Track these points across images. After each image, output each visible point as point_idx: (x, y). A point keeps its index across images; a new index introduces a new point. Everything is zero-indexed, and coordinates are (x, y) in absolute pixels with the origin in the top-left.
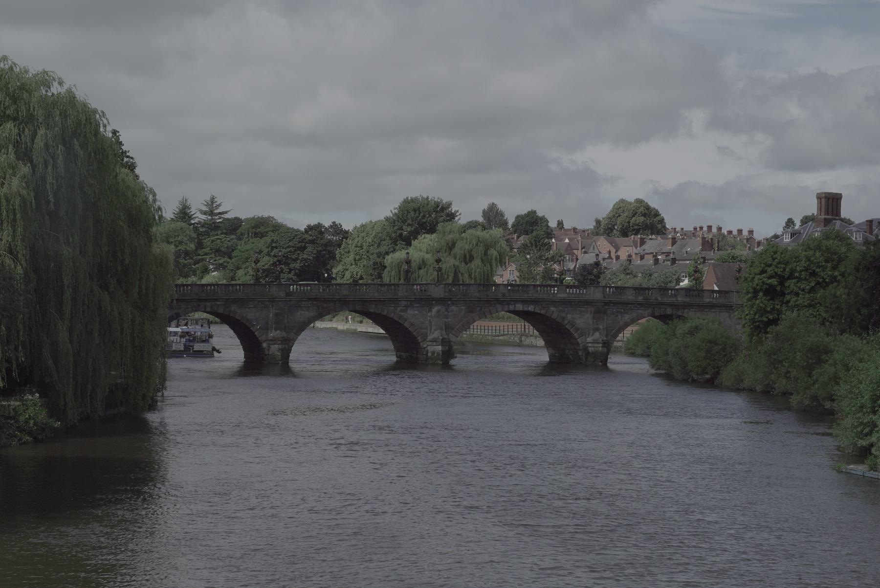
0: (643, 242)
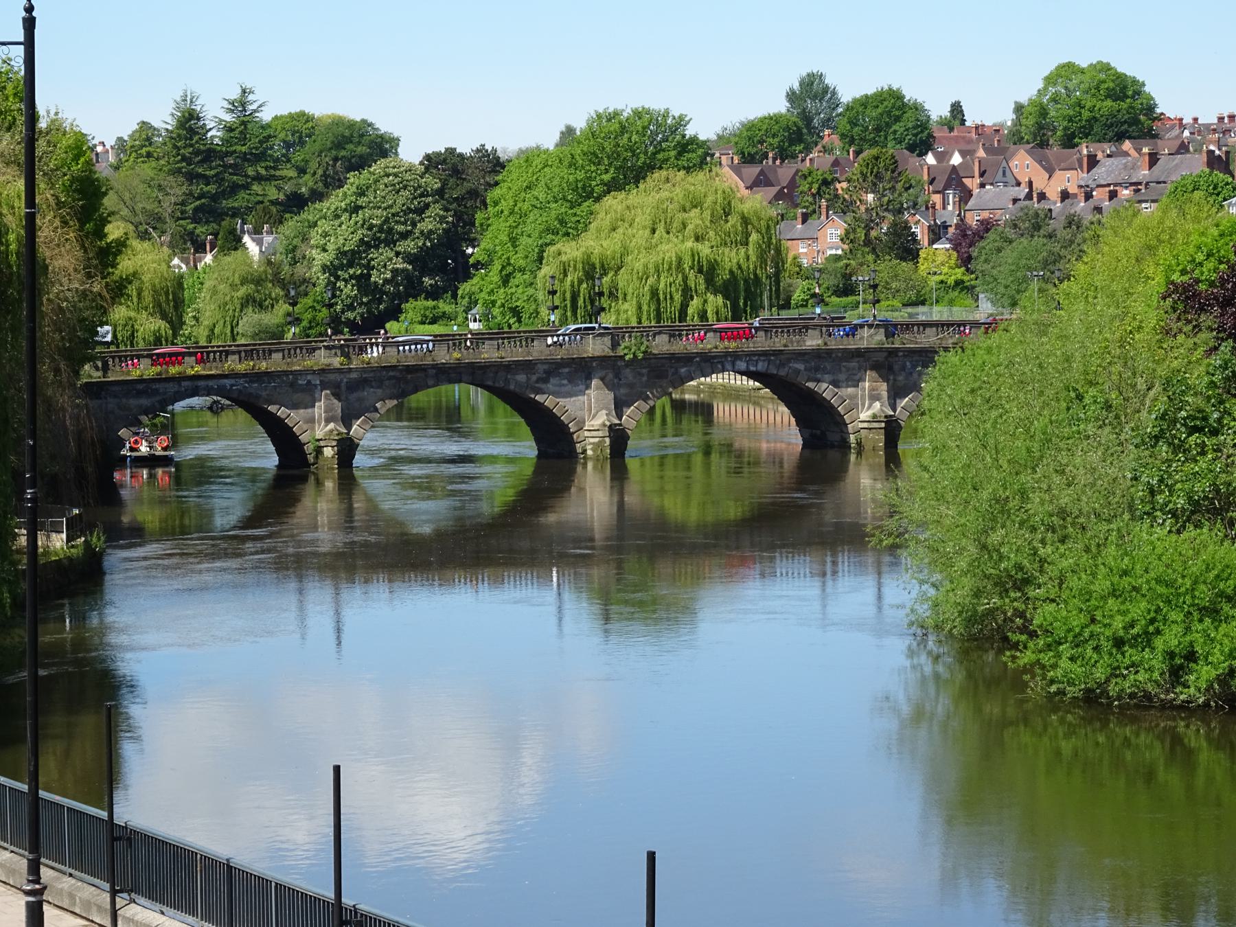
0: (1093, 162)
